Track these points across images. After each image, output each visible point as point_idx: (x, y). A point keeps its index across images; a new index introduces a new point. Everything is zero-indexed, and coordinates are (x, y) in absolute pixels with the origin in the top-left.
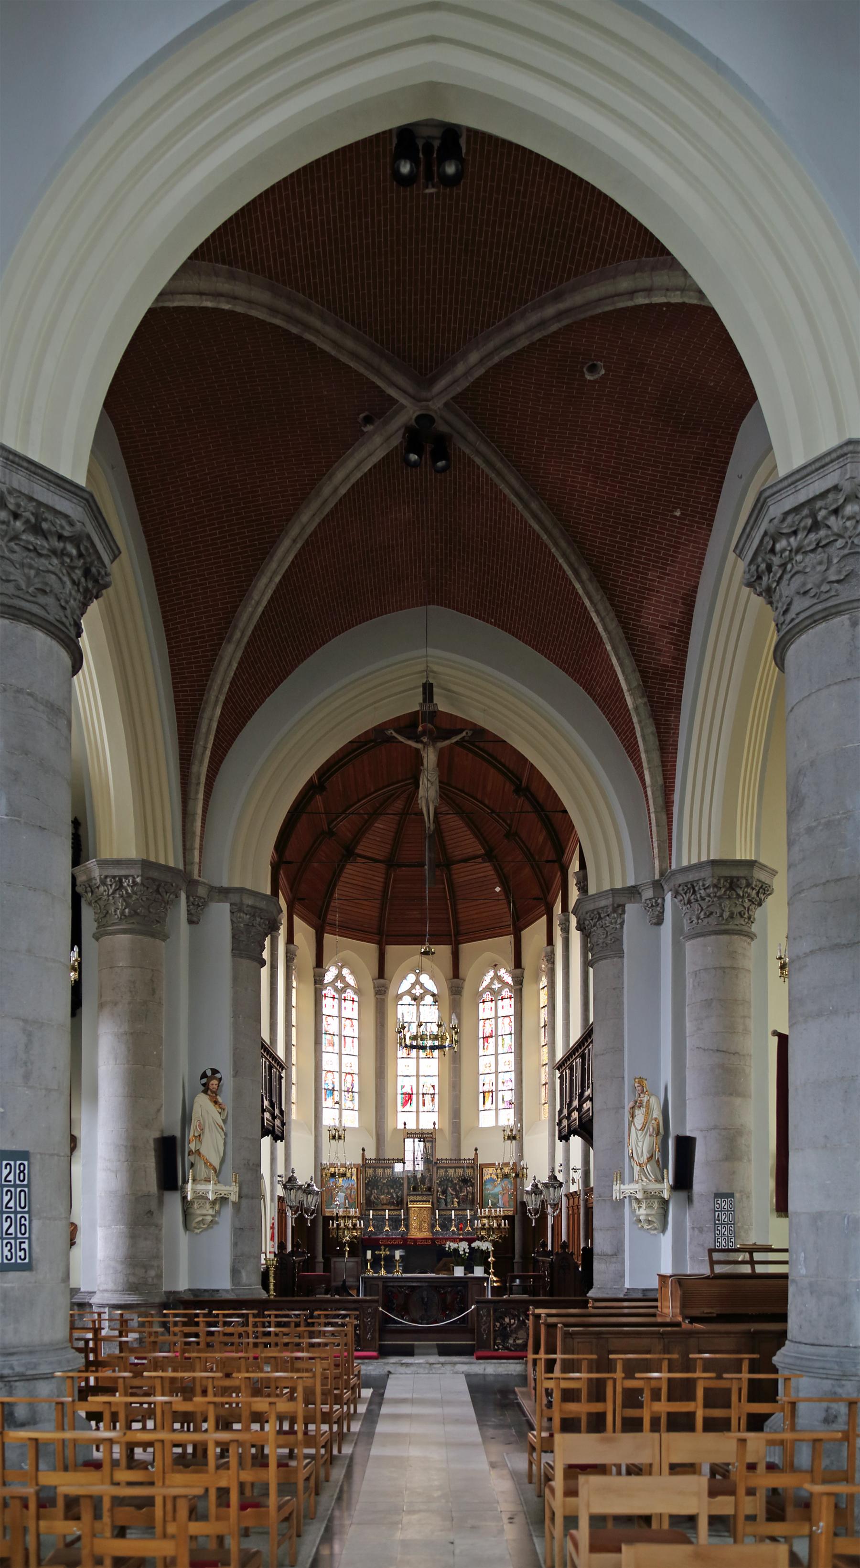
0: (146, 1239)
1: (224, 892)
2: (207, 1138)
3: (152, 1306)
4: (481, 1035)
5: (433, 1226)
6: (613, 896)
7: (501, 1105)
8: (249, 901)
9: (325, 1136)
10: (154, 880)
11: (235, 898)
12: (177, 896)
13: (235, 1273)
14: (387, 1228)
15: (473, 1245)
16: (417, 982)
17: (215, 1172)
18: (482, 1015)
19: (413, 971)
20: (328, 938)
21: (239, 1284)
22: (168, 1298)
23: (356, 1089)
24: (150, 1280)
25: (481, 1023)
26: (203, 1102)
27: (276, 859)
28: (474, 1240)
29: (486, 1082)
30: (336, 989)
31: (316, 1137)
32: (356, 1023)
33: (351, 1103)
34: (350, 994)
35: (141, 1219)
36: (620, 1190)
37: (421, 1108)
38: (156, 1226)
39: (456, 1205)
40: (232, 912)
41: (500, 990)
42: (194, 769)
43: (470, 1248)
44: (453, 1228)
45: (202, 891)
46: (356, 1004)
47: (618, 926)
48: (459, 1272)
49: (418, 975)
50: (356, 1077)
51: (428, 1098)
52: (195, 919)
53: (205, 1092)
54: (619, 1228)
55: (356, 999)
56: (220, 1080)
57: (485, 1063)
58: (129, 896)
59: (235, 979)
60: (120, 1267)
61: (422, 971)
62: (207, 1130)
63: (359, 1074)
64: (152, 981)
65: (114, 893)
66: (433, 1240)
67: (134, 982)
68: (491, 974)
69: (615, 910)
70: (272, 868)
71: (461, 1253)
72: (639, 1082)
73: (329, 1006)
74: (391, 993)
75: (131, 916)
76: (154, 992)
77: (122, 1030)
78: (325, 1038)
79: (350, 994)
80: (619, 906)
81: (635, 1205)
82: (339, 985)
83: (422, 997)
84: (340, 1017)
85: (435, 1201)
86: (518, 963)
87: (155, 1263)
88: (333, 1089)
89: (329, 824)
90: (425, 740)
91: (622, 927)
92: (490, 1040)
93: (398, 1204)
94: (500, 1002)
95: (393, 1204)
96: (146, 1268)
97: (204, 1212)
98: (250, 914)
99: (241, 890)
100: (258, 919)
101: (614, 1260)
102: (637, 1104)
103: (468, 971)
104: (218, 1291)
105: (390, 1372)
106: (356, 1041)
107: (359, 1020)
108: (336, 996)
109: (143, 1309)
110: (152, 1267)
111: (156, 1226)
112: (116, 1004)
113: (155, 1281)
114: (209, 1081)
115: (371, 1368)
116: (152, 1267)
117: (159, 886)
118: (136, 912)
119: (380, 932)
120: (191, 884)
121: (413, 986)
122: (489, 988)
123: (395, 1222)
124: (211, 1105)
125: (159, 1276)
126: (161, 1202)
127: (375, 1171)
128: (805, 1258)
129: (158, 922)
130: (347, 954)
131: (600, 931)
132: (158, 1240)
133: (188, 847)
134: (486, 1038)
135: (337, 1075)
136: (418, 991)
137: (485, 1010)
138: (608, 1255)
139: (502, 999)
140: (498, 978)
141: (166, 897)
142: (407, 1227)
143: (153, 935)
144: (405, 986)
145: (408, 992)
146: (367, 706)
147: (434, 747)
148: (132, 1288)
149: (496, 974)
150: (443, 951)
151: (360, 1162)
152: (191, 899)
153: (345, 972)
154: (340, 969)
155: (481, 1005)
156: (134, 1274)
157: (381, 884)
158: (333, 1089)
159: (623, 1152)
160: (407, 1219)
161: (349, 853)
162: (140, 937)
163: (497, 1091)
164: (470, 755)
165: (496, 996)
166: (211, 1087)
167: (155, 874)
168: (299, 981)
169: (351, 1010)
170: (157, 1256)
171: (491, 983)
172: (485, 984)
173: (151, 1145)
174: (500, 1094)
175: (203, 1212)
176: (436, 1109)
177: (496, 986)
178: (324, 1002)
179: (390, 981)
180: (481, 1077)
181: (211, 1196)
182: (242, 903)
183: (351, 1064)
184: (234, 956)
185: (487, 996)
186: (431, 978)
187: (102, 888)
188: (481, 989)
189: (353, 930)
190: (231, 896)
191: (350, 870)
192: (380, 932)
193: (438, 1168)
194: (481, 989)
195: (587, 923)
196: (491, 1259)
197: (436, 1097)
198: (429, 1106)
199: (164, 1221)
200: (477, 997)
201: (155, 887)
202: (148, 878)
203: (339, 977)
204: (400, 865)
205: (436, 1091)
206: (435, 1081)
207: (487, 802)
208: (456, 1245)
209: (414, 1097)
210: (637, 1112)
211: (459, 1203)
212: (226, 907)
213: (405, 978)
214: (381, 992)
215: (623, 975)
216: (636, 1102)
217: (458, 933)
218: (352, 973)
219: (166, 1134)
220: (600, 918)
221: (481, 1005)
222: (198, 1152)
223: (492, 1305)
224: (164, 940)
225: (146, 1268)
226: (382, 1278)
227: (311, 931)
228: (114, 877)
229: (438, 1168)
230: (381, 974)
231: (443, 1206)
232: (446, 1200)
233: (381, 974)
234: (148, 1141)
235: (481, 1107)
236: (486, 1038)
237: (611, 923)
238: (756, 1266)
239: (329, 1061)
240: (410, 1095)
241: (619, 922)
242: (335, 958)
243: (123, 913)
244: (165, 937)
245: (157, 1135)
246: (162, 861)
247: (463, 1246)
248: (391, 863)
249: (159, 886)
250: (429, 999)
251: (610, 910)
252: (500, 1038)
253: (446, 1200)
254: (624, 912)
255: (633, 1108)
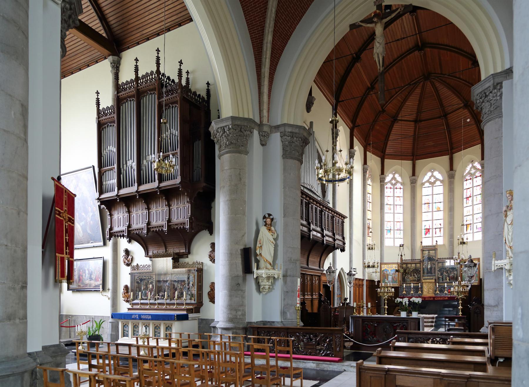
0: (236, 297)
1: (277, 127)
2: (264, 247)
3: (239, 329)
4: (465, 197)
5: (436, 291)
6: (494, 79)
7: (475, 230)
8: (289, 130)
9: (366, 248)
10: (238, 125)
11: (282, 129)
12: (252, 133)
13: (283, 313)
14: (412, 292)
15: (411, 300)
16: (432, 176)
17: (270, 264)
18: (465, 187)
19: (430, 171)
20: (386, 161)
21: (286, 319)
22: (247, 325)
23: (402, 229)
24: (238, 316)
25: (465, 191)
26: (263, 230)
27: (352, 126)
28: (411, 298)
29: (468, 220)
30: (392, 184)
31: (381, 251)
32: (402, 198)
33: (400, 234)
34: (399, 186)
35: (236, 287)
36: (497, 263)
37: (434, 235)
38: (242, 291)
39: (448, 280)
40: (281, 137)
41: (475, 173)
42: (263, 70)
43: (409, 301)
44: (446, 292)
45: (266, 129)
46: (402, 190)
47: (498, 98)
48: (403, 314)
49: (432, 172)
50: (402, 223)
51: (438, 230)
52: (264, 143)
53: (265, 225)
54: (499, 288)
55: (402, 187)
56: (272, 219)
57: (467, 211)
58: (228, 135)
59: (285, 170)
60: (225, 310)
61: (435, 170)
62: (264, 244)
63: (403, 222)
64: (240, 174)
65: (222, 135)
66: (434, 298)
67: (231, 176)
68: (470, 166)
69: (495, 88)
70: (350, 130)
71: (404, 304)
72: (509, 193)
73: (388, 192)
74: (419, 182)
75: (229, 145)
76: (240, 179)
77: (226, 199)
78: (386, 208)
79: (399, 186)
80: (498, 84)
81: (507, 274)
82: (393, 182)
83: (435, 182)
84: (394, 196)
85: (437, 279)
86: (483, 159)
87: (241, 308)
88: (391, 230)
89: (382, 108)
90: (375, 20)
91: (501, 98)
92: (470, 198)
93: (418, 281)
94: (475, 180)
95: (415, 280)
96: (236, 310)
97: (264, 284)
98: (290, 136)
99: (285, 125)
100: (295, 138)
101: (496, 309)
102: (510, 208)
103: (457, 166)
104: (274, 322)
105: (345, 370)
106: (402, 206)
107: (403, 197)
108: (392, 187)
109: (235, 330)
110: (239, 310)
111: (242, 291)
112: (224, 187)
113: (241, 317)
114: (269, 220)
115: (335, 367)
116: (239, 310)
117: (241, 128)
118: (231, 143)
119: (413, 155)
120: (260, 126)
121: (430, 177)
122: (469, 173)
123: (416, 289)
124: (267, 231)
125: (244, 315)
126: (244, 279)
127: (407, 266)
128: (522, 315)
129: (242, 146)
130: (398, 167)
131: (487, 104)
132: (243, 297)
133: (261, 109)
134: (467, 198)
135: (392, 223)
136: (432, 180)
137: (467, 184)
138: (492, 306)
139: (476, 177)
140: (474, 167)
141: (245, 133)
142: (422, 291)
143: (240, 152)
144: (426, 178)
145: (428, 181)
146: (346, 16)
147: (381, 23)
148: (230, 320)
149: (473, 165)
150: (445, 159)
151: (399, 261)
152: (261, 133)
153: (397, 176)
154: (394, 175)
155: (465, 182)
156: (231, 313)
157: (413, 132)
158: (391, 230)
159: (503, 240)
160: (422, 288)
161: (395, 119)
162: (234, 154)
163: (473, 223)
164: (449, 53)
165: (472, 176)
166: (267, 222)
167: (239, 123)
168: (372, 181)
169: (399, 192)
170: (243, 305)
171: (470, 170)
172: (467, 171)
173: (239, 252)
174: (475, 225)
175: (265, 284)
176: (442, 235)
177: (473, 171)
178: (386, 190)
179: (418, 177)
180: (465, 218)
181: (264, 276)
182: (285, 131)
183: (400, 217)
184: (283, 158)
185: (468, 177)
186: (439, 173)
187: (218, 134)
188: (465, 174)
189: (399, 156)
190: (280, 128)
191: (396, 127)
192: (413, 155)
193: (438, 263)
194: (465, 174)
195: (478, 101)
196: (460, 307)
197: (442, 229)
198: (438, 234)
199: (247, 288)
200: (463, 179)
201: (239, 129)
202: (235, 125)
203: (394, 178)
204: (421, 121)
205: (442, 226)
206: (441, 222)
207: (461, 77)
208: (401, 300)
209: (431, 230)
210: (508, 213)
211: (449, 279)
212: (278, 135)
213: (426, 175)
214: (413, 182)
215: (502, 128)
216: (508, 207)
217: (452, 148)
218: (401, 175)
219: (247, 247)
220: (486, 96)
221: (465, 182)
222: (261, 254)
223: (407, 335)
224: (247, 155)
225: (236, 310)
226: (363, 318)
227: (379, 159)
228: (221, 128)
229: (438, 263)
230: (414, 174)
231: (441, 281)
232: (442, 278)
233: (414, 174)
234: (237, 250)
235: (465, 232)
236: (467, 198)
237: (494, 97)
238: (120, 348)
239: (388, 217)
240: (429, 229)
241: (498, 94)
242: (390, 170)
243: (226, 144)
244: (247, 153)
245: (242, 247)
246: (241, 116)
247: (406, 300)
248: (416, 121)
249: (241, 128)
250: (438, 183)
251: (491, 88)
252: (475, 197)
253: (442, 278)
254: (501, 87)
255: (506, 211)
